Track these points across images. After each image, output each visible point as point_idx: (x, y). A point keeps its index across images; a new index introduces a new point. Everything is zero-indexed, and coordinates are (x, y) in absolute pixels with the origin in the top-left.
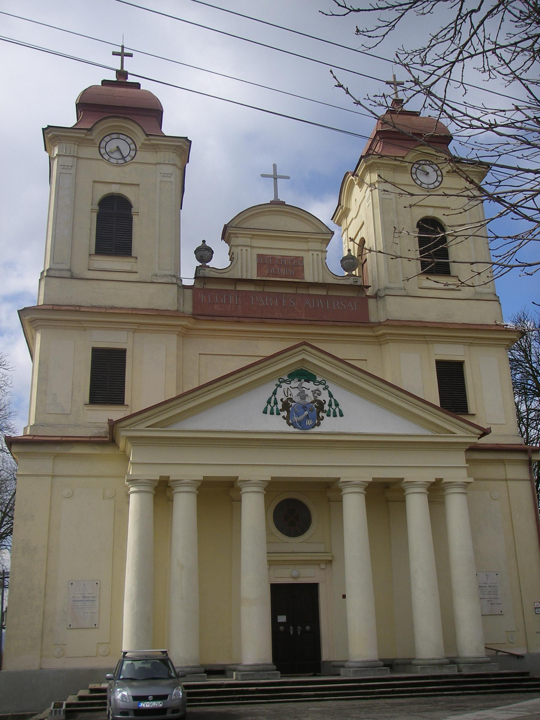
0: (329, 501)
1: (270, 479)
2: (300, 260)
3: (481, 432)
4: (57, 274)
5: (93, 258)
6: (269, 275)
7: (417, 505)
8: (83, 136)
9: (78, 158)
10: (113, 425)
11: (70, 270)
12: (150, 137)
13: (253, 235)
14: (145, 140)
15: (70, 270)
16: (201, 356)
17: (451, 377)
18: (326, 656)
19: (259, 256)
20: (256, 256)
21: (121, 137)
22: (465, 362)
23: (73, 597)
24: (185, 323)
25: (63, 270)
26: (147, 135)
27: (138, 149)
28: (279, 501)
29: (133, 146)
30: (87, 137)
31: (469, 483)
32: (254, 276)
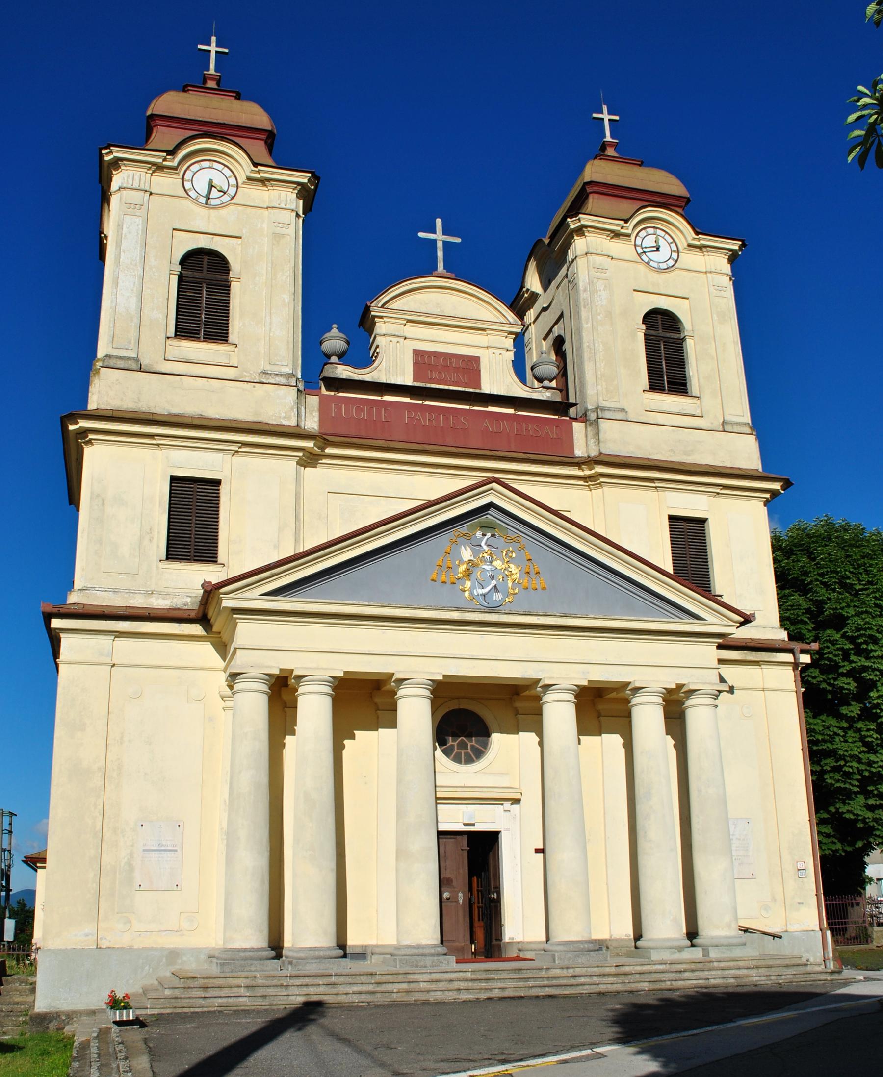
0: (517, 713)
1: (342, 675)
2: (474, 361)
3: (743, 620)
4: (120, 364)
5: (169, 342)
6: (431, 381)
7: (648, 717)
8: (160, 161)
9: (151, 194)
10: (211, 592)
11: (137, 360)
12: (260, 168)
13: (409, 321)
14: (252, 171)
15: (137, 360)
16: (698, 413)
17: (689, 535)
18: (507, 938)
19: (417, 353)
20: (411, 352)
21: (216, 165)
22: (709, 520)
23: (145, 845)
24: (309, 444)
25: (129, 358)
26: (255, 165)
27: (240, 185)
28: (448, 710)
29: (233, 181)
30: (165, 163)
31: (720, 692)
32: (408, 380)
